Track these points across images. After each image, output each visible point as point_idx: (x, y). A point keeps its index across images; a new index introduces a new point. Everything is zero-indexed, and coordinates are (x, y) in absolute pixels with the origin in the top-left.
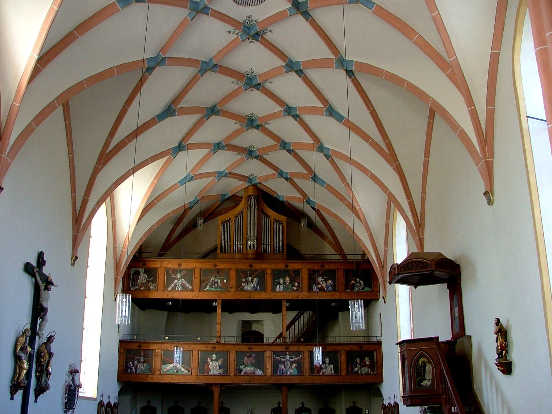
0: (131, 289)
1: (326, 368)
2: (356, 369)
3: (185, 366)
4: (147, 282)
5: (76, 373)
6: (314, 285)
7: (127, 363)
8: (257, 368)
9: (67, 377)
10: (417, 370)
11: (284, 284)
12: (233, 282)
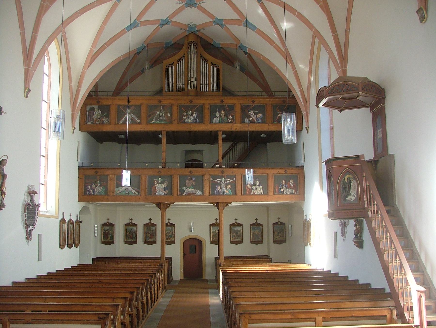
0: (88, 123)
1: (256, 189)
2: (282, 190)
3: (134, 188)
4: (101, 116)
5: (34, 194)
6: (246, 118)
7: (86, 186)
8: (197, 189)
9: (26, 197)
10: (343, 186)
11: (220, 117)
12: (176, 115)
